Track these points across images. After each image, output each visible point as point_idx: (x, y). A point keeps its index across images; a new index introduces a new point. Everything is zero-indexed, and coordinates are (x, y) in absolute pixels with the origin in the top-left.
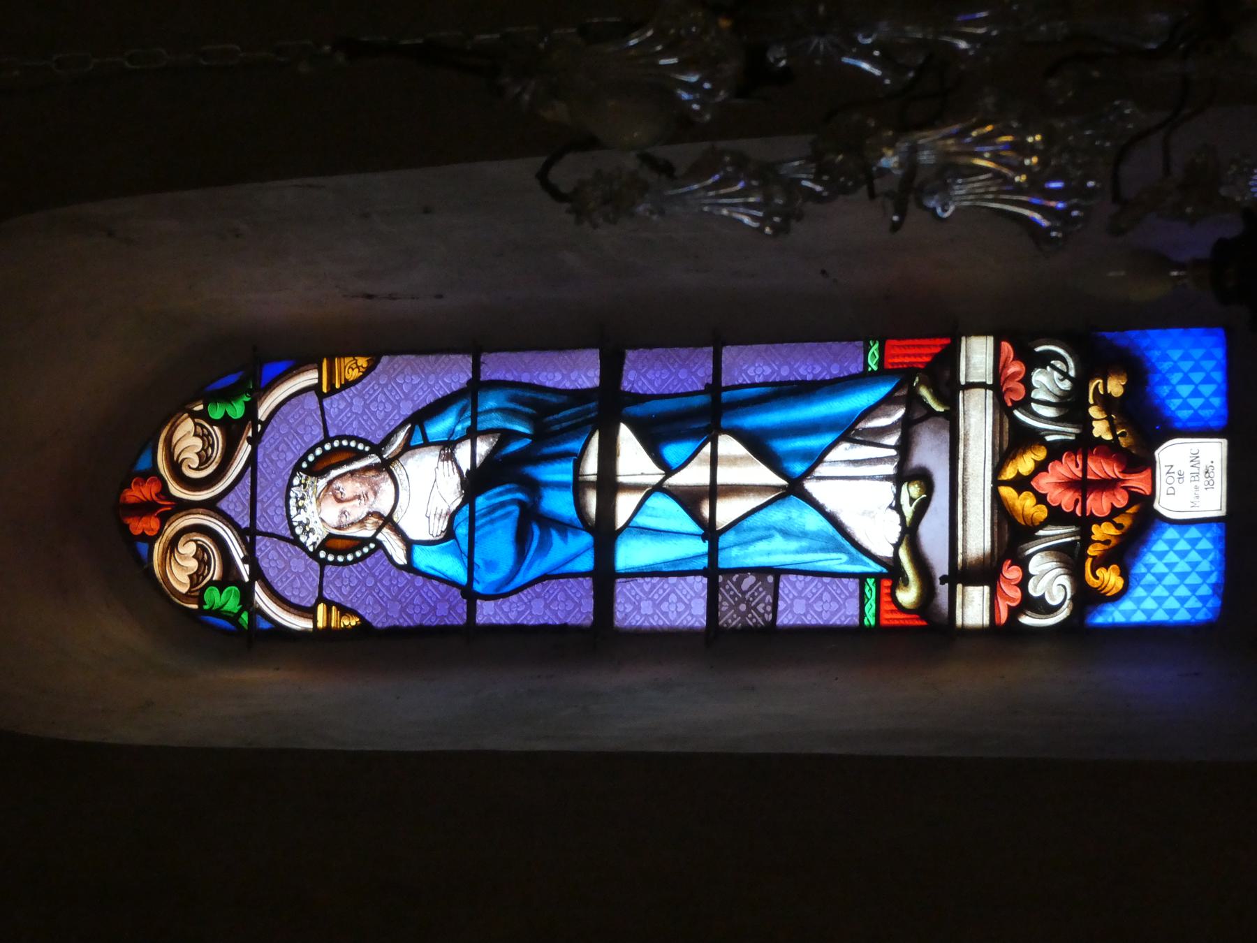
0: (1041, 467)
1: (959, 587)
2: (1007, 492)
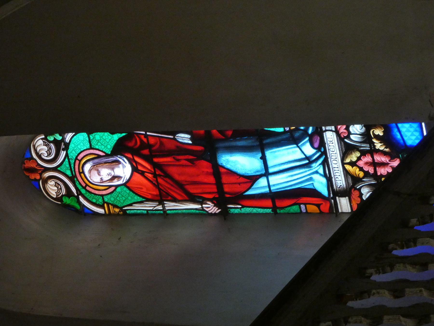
0: (359, 159)
1: (337, 198)
2: (348, 167)
